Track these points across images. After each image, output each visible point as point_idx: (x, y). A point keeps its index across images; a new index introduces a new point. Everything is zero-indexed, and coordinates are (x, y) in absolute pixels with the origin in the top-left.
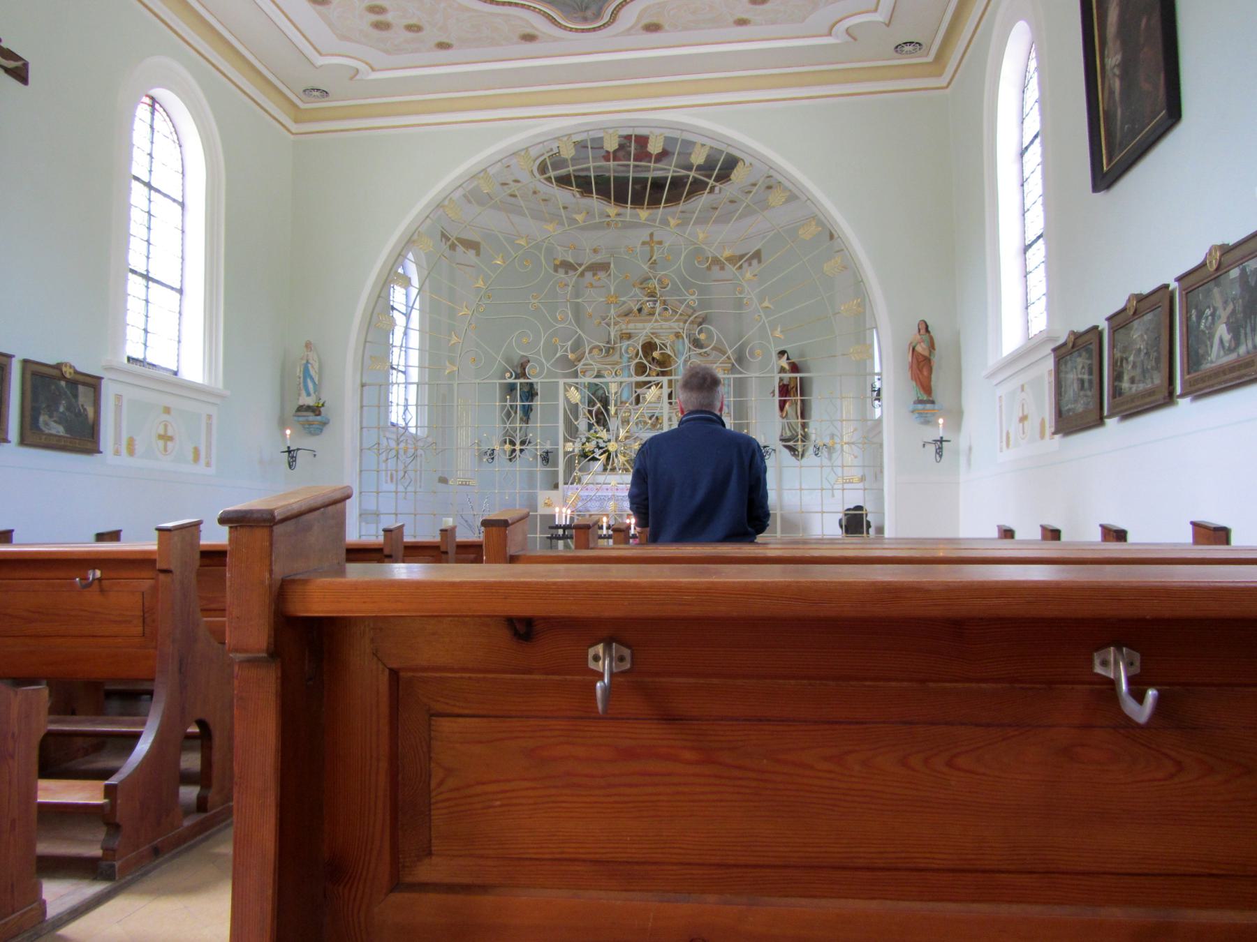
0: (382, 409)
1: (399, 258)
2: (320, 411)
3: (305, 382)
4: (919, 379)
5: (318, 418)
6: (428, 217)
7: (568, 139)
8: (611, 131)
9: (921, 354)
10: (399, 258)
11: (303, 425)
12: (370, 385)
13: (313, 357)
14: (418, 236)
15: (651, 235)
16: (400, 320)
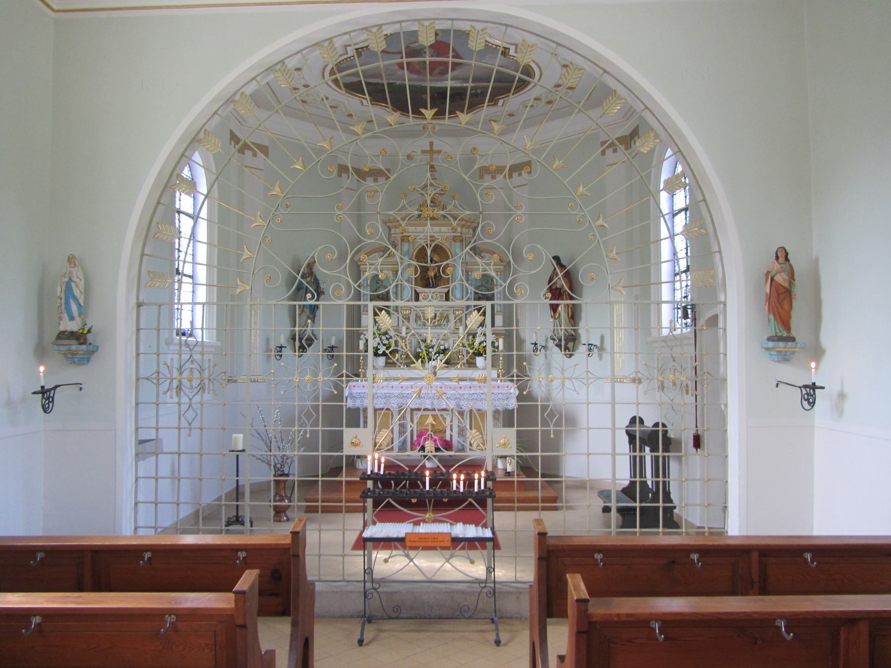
0: (165, 309)
1: (183, 158)
2: (85, 339)
3: (67, 303)
4: (779, 313)
5: (84, 347)
6: (216, 113)
7: (378, 30)
8: (426, 23)
9: (781, 285)
10: (183, 158)
11: (65, 355)
12: (149, 304)
13: (77, 274)
14: (241, 97)
15: (431, 144)
16: (185, 225)
